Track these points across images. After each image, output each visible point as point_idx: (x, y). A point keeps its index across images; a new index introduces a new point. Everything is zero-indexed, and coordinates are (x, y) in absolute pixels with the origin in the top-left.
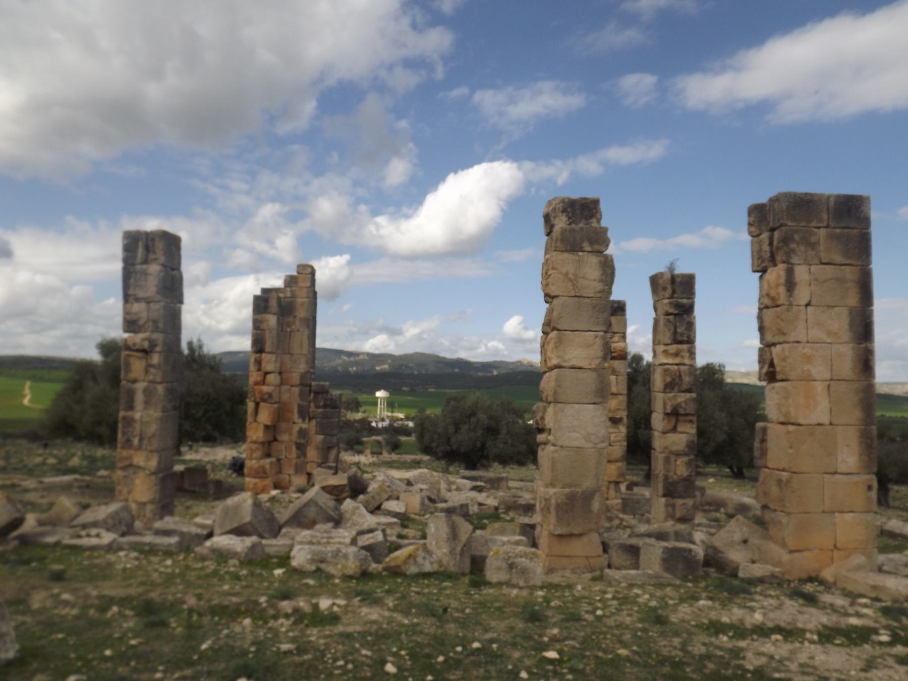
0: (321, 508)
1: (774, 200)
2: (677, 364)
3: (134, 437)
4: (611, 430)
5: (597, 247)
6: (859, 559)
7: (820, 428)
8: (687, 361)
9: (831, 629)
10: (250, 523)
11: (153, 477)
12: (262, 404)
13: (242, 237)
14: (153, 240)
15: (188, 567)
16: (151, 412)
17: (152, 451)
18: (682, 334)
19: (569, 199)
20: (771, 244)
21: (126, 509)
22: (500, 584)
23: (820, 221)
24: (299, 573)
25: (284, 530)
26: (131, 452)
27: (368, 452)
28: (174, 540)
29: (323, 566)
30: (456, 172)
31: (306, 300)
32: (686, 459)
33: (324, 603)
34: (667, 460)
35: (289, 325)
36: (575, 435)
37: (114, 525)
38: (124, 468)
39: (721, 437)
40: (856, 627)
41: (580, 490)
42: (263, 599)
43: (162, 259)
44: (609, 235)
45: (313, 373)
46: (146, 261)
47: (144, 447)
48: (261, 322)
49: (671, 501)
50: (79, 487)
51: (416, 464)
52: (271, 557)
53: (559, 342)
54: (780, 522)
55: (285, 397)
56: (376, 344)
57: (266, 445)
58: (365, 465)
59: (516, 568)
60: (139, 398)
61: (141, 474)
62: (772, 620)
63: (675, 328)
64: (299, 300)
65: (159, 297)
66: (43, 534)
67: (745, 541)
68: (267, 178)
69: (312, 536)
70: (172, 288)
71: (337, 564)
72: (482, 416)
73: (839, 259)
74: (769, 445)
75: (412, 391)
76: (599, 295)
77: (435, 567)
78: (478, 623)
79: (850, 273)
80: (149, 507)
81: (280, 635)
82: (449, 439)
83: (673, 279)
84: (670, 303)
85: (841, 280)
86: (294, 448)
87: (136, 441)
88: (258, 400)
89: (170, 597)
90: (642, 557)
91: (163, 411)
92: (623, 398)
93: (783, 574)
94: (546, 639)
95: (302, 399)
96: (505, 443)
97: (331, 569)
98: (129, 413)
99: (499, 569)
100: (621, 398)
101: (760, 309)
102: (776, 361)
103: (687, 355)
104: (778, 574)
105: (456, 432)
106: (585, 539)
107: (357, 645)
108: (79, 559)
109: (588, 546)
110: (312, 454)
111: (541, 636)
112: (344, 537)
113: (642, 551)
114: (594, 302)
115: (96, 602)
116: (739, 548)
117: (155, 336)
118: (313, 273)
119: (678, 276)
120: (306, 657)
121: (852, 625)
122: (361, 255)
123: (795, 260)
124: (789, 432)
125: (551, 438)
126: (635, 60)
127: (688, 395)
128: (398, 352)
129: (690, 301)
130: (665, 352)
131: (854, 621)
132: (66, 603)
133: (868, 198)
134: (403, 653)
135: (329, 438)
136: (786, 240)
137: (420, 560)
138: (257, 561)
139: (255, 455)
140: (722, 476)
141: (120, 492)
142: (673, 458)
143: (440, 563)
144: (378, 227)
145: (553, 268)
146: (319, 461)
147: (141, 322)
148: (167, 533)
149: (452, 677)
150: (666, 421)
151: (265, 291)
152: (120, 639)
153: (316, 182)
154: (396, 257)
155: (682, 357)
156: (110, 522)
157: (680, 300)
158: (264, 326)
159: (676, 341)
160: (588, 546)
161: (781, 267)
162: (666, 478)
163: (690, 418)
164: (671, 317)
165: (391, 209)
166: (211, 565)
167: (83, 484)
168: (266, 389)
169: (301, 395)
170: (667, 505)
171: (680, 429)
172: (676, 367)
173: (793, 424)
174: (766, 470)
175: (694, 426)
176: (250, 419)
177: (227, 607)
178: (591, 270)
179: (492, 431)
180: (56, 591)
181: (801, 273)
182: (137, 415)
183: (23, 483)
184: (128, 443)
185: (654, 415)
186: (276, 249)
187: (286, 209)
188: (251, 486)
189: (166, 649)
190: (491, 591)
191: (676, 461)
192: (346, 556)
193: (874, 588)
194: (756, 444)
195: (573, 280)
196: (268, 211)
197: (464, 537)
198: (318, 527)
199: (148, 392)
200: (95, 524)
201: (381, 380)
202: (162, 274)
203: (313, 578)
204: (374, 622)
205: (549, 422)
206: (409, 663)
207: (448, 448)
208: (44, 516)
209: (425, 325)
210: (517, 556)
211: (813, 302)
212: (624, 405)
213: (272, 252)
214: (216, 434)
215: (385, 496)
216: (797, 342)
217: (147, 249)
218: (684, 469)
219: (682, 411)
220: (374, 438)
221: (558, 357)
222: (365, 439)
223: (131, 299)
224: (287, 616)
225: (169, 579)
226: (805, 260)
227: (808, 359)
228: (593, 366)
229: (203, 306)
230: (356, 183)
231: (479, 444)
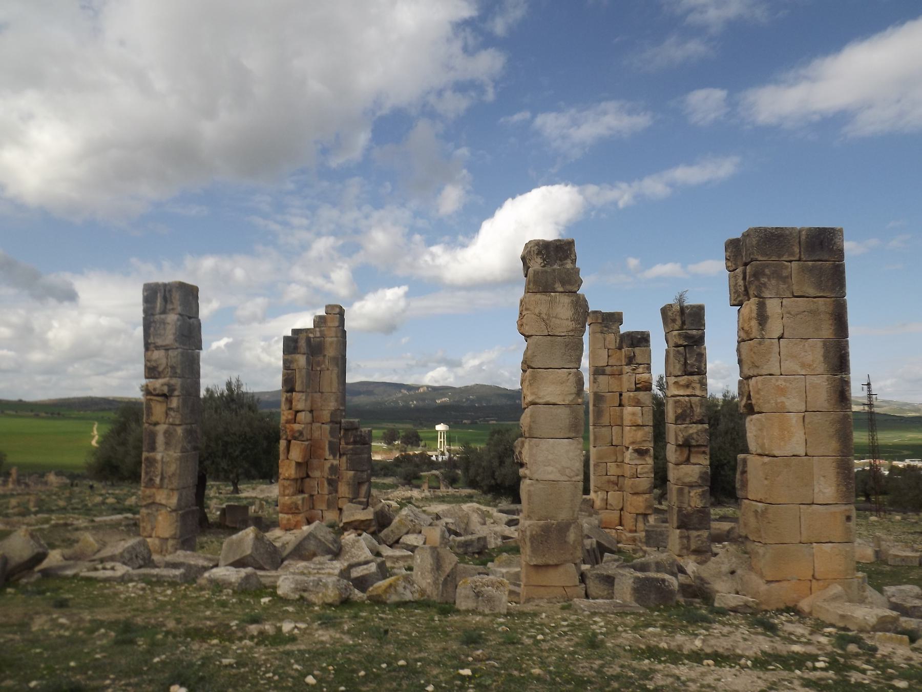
0: (320, 541)
1: (747, 235)
2: (688, 396)
3: (156, 476)
4: (638, 462)
5: (569, 288)
6: (837, 589)
8: (698, 392)
9: (769, 655)
10: (250, 555)
11: (174, 514)
12: (293, 442)
13: (297, 272)
14: (170, 291)
15: (185, 596)
16: (171, 453)
17: (172, 490)
18: (692, 366)
19: (543, 241)
20: (744, 278)
21: (144, 544)
22: (467, 611)
23: (792, 254)
24: (285, 601)
25: (286, 563)
26: (154, 490)
27: (425, 486)
28: (177, 572)
29: (305, 595)
30: (513, 197)
31: (335, 339)
32: (700, 490)
33: (287, 627)
34: (680, 492)
35: (319, 364)
36: (550, 469)
37: (131, 559)
38: (147, 506)
40: (797, 653)
41: (555, 522)
42: (233, 623)
43: (179, 309)
45: (344, 410)
46: (164, 312)
48: (291, 362)
49: (686, 533)
50: (127, 526)
51: (469, 498)
52: (266, 587)
53: (534, 379)
54: (757, 553)
55: (317, 434)
56: (435, 376)
57: (299, 482)
58: (417, 499)
59: (483, 596)
60: (160, 440)
61: (163, 511)
62: (712, 646)
64: (329, 340)
65: (177, 345)
66: (64, 568)
67: (733, 573)
68: (327, 213)
69: (306, 567)
70: (191, 335)
71: (318, 593)
73: (812, 291)
74: (749, 476)
75: (473, 423)
76: (572, 334)
77: (417, 596)
78: (418, 644)
80: (171, 542)
81: (230, 652)
82: (494, 472)
83: (682, 310)
84: (679, 335)
85: (814, 313)
86: (326, 484)
87: (158, 480)
88: (289, 438)
89: (153, 621)
90: (616, 587)
91: (182, 452)
92: (649, 430)
93: (757, 604)
94: (470, 659)
95: (332, 436)
97: (312, 598)
98: (151, 454)
99: (467, 597)
100: (646, 429)
101: (739, 342)
103: (698, 386)
104: (751, 604)
105: (500, 465)
106: (561, 570)
107: (292, 661)
108: (91, 589)
109: (565, 576)
110: (344, 490)
111: (468, 656)
112: (336, 568)
113: (616, 581)
114: (567, 340)
115: (88, 625)
116: (725, 578)
117: (173, 381)
118: (341, 313)
119: (687, 307)
120: (242, 670)
121: (793, 652)
122: (421, 287)
125: (527, 472)
126: (698, 75)
127: (700, 426)
128: (458, 385)
129: (700, 332)
130: (676, 383)
131: (796, 648)
132: (62, 626)
133: (841, 231)
134: (331, 668)
135: (359, 473)
136: (756, 275)
137: (400, 589)
138: (250, 590)
139: (287, 492)
141: (144, 528)
142: (686, 489)
143: (423, 592)
144: (433, 256)
145: (527, 309)
146: (351, 496)
147: (160, 369)
148: (175, 566)
149: (364, 689)
150: (678, 453)
151: (295, 331)
152: (88, 653)
153: (376, 215)
154: (454, 288)
155: (693, 388)
156: (127, 556)
158: (294, 366)
160: (565, 576)
161: (754, 300)
162: (680, 509)
163: (703, 449)
164: (681, 349)
165: (447, 238)
166: (206, 594)
167: (131, 522)
168: (296, 427)
169: (332, 432)
170: (681, 537)
171: (693, 460)
172: (687, 399)
173: (767, 455)
174: (746, 501)
175: (708, 457)
176: (282, 457)
177: (201, 629)
180: (55, 616)
181: (773, 306)
182: (159, 456)
183: (75, 522)
184: (150, 483)
185: (669, 446)
186: (332, 282)
187: (340, 242)
188: (285, 522)
189: (123, 661)
190: (456, 618)
191: (689, 492)
192: (326, 586)
193: (843, 617)
194: (738, 476)
195: (545, 321)
196: (322, 245)
197: (448, 568)
198: (316, 559)
199: (168, 434)
200: (112, 558)
201: (441, 414)
202: (179, 323)
203: (294, 606)
204: (322, 642)
205: (526, 458)
206: (332, 676)
207: (493, 481)
208: (68, 552)
209: (486, 356)
210: (484, 585)
211: (785, 336)
212: (651, 436)
213: (328, 286)
214: (253, 472)
215: (405, 531)
216: (771, 375)
217: (165, 300)
218: (698, 501)
219: (694, 443)
220: (434, 472)
221: (533, 394)
222: (422, 474)
224: (252, 638)
225: (162, 606)
227: (782, 391)
228: (567, 402)
229: (262, 343)
230: (417, 214)
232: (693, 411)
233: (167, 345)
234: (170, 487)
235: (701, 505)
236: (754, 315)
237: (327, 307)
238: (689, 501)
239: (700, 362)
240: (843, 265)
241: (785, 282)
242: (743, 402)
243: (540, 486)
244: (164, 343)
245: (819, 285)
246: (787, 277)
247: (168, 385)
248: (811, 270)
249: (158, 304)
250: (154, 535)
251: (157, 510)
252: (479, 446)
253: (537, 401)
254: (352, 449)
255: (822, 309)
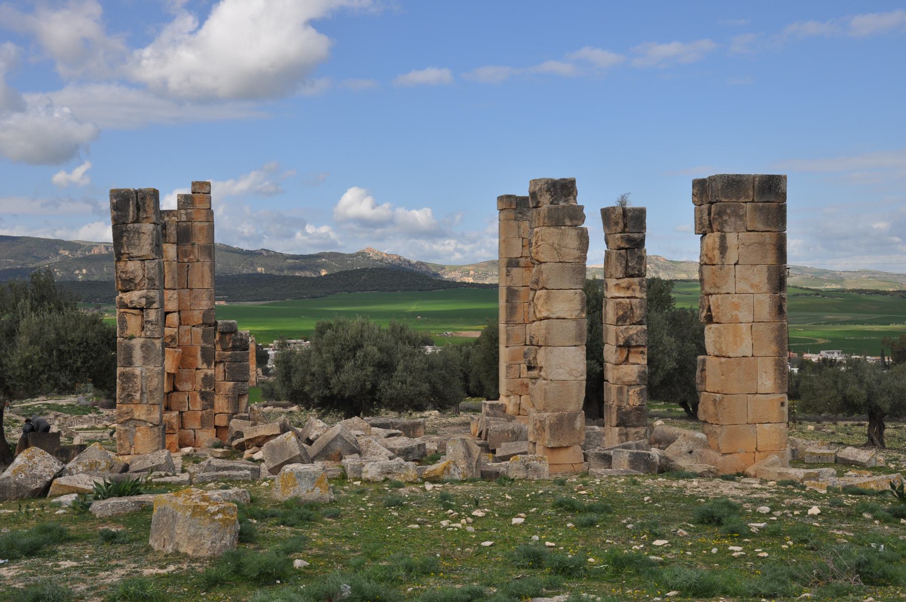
0: (346, 442)
2: (628, 298)
5: (575, 222)
7: (744, 359)
11: (156, 429)
16: (151, 367)
18: (633, 268)
19: (552, 180)
20: (709, 214)
23: (747, 197)
26: (132, 406)
29: (389, 476)
34: (620, 391)
36: (561, 371)
39: (670, 365)
44: (585, 212)
46: (137, 221)
47: (145, 401)
49: (624, 430)
60: (138, 354)
63: (627, 262)
64: (197, 225)
67: (691, 452)
72: (371, 349)
73: (761, 227)
76: (577, 261)
79: (769, 238)
82: (327, 381)
83: (625, 212)
84: (622, 238)
85: (762, 244)
86: (198, 398)
87: (137, 396)
95: (205, 341)
96: (404, 382)
101: (701, 265)
102: (712, 308)
106: (570, 450)
117: (152, 293)
119: (629, 210)
123: (727, 229)
124: (721, 363)
127: (639, 327)
129: (641, 235)
130: (617, 285)
133: (785, 177)
136: (720, 214)
137: (452, 470)
140: (672, 418)
142: (626, 388)
147: (137, 281)
150: (618, 353)
157: (631, 235)
159: (628, 275)
162: (619, 408)
163: (641, 349)
164: (623, 251)
169: (205, 336)
171: (631, 360)
172: (628, 300)
175: (646, 357)
178: (571, 241)
179: (385, 367)
182: (137, 371)
184: (129, 398)
185: (606, 347)
191: (628, 391)
194: (698, 373)
217: (138, 208)
218: (636, 400)
221: (548, 310)
223: (124, 258)
226: (735, 229)
227: (736, 306)
231: (369, 386)
232: (633, 313)
233: (143, 256)
234: (150, 402)
235: (639, 403)
236: (717, 246)
237: (194, 184)
238: (628, 399)
239: (641, 264)
240: (785, 206)
241: (741, 220)
242: (704, 314)
243: (553, 385)
244: (140, 254)
245: (766, 222)
246: (742, 215)
247: (147, 298)
248: (761, 210)
249: (131, 213)
250: (132, 452)
251: (135, 426)
252: (300, 345)
253: (551, 316)
254: (230, 356)
255: (768, 241)
